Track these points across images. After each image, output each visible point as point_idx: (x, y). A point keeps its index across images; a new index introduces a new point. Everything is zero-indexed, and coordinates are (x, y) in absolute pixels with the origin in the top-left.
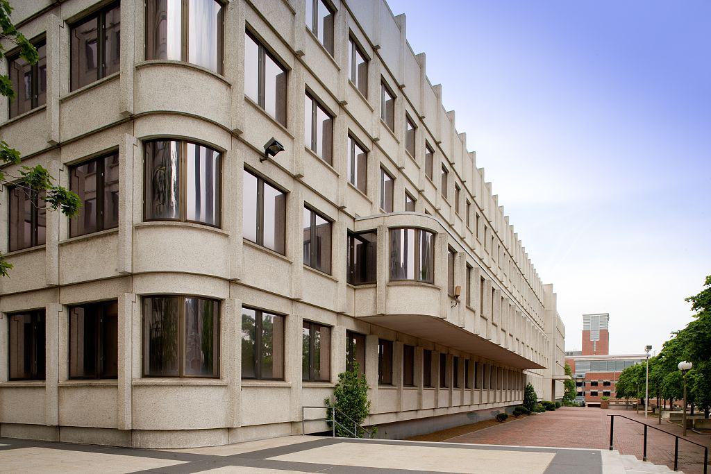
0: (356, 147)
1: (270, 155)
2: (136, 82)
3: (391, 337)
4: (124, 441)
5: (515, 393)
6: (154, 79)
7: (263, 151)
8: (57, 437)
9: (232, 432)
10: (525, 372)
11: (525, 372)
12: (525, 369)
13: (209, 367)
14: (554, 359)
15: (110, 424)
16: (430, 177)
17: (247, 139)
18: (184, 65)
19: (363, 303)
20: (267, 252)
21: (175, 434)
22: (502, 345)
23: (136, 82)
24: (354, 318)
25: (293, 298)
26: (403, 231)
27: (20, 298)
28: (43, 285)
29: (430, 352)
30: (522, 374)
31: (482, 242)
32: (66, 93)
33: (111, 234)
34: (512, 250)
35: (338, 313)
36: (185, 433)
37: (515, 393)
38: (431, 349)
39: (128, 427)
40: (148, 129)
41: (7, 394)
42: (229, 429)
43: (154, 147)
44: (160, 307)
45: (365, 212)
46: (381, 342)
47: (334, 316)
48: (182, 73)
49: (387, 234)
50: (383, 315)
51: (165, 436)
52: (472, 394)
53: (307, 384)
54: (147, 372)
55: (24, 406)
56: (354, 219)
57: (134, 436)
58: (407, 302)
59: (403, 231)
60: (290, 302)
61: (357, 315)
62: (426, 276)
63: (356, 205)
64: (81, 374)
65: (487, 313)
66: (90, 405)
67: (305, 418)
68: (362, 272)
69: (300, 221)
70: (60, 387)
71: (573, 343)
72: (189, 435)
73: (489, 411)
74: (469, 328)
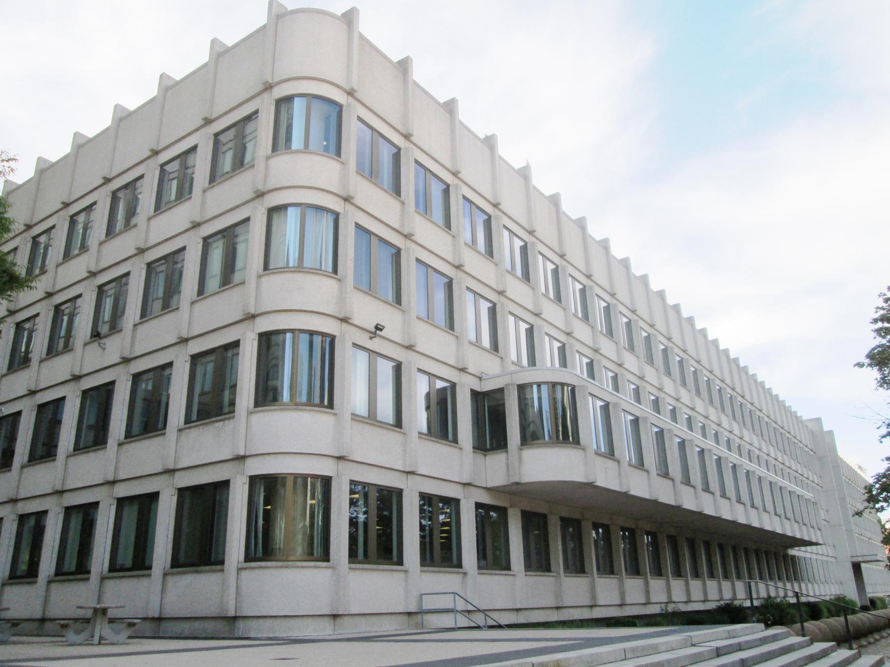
0: (515, 239)
1: (378, 332)
2: (258, 287)
3: (541, 508)
4: (227, 627)
5: (807, 585)
6: (271, 282)
7: (374, 330)
8: (157, 627)
9: (339, 621)
13: (319, 549)
15: (212, 611)
17: (356, 322)
18: (300, 268)
19: (495, 470)
20: (382, 425)
21: (278, 621)
25: (407, 470)
26: (535, 387)
27: (134, 482)
28: (160, 469)
30: (786, 556)
32: (195, 297)
33: (229, 419)
35: (465, 485)
36: (288, 619)
37: (807, 585)
39: (231, 613)
40: (265, 325)
41: (8, 589)
42: (335, 616)
43: (268, 342)
44: (268, 487)
45: (490, 372)
47: (460, 488)
48: (298, 277)
49: (516, 392)
50: (518, 483)
51: (268, 622)
52: (767, 585)
53: (353, 566)
55: (23, 601)
56: (480, 378)
57: (237, 624)
58: (545, 465)
59: (535, 387)
60: (405, 475)
61: (490, 484)
66: (195, 591)
67: (425, 607)
68: (491, 433)
69: (419, 389)
70: (165, 575)
72: (292, 622)
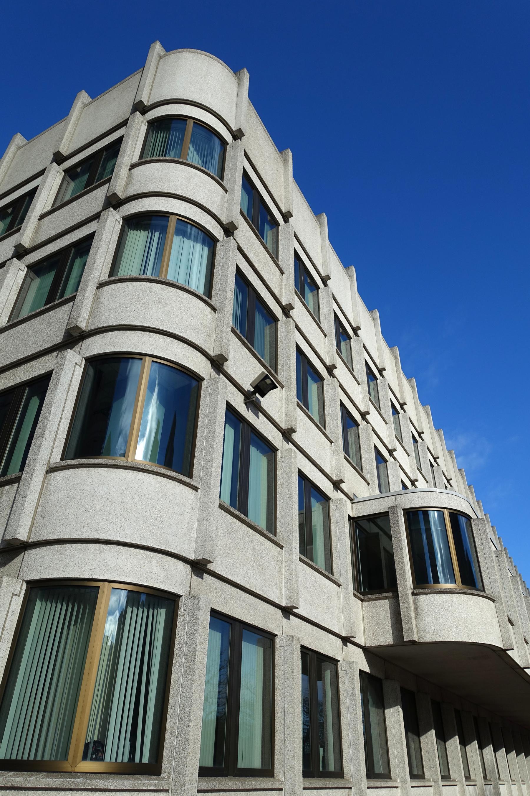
23: (96, 299)
68: (374, 577)
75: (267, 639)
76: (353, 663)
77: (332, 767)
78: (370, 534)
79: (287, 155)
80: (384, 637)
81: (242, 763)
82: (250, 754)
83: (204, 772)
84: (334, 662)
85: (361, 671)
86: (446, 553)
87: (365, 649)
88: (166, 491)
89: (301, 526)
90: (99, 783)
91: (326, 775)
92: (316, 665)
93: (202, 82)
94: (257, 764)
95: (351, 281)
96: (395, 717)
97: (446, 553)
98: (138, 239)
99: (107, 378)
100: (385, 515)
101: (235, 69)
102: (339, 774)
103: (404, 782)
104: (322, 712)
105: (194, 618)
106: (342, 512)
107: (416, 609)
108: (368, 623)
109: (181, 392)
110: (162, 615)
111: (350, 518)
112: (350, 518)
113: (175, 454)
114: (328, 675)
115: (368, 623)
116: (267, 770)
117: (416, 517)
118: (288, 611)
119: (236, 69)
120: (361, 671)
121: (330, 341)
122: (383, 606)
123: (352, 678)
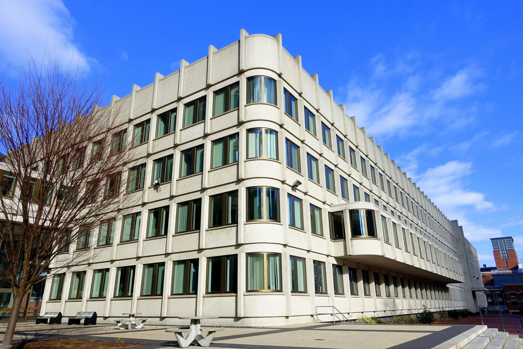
3: (354, 266)
10: (448, 286)
11: (448, 286)
12: (447, 283)
14: (470, 275)
16: (383, 189)
20: (297, 229)
22: (435, 272)
23: (245, 166)
24: (335, 257)
29: (378, 274)
31: (401, 202)
34: (418, 199)
38: (377, 272)
45: (335, 202)
46: (350, 269)
54: (210, 291)
62: (372, 233)
63: (330, 198)
64: (150, 294)
65: (435, 261)
68: (338, 233)
71: (486, 258)
73: (415, 315)
74: (400, 259)
75: (303, 259)
76: (330, 262)
77: (324, 291)
78: (336, 220)
79: (299, 58)
80: (341, 254)
81: (300, 290)
82: (301, 288)
83: (292, 292)
84: (324, 263)
85: (333, 264)
86: (366, 224)
87: (335, 257)
88: (273, 227)
89: (311, 215)
90: (268, 293)
91: (322, 293)
92: (318, 264)
93: (264, 53)
94: (303, 290)
95: (330, 98)
96: (346, 277)
97: (366, 224)
98: (252, 136)
99: (253, 193)
100: (342, 212)
101: (274, 35)
102: (326, 293)
103: (348, 296)
104: (320, 273)
105: (286, 259)
106: (326, 210)
107: (352, 245)
108: (336, 249)
109: (273, 193)
110: (278, 258)
111: (329, 212)
112: (329, 212)
113: (275, 216)
114: (322, 266)
115: (336, 249)
116: (306, 292)
117: (354, 213)
118: (308, 251)
119: (275, 36)
120: (333, 264)
121: (320, 142)
122: (341, 243)
123: (330, 267)
